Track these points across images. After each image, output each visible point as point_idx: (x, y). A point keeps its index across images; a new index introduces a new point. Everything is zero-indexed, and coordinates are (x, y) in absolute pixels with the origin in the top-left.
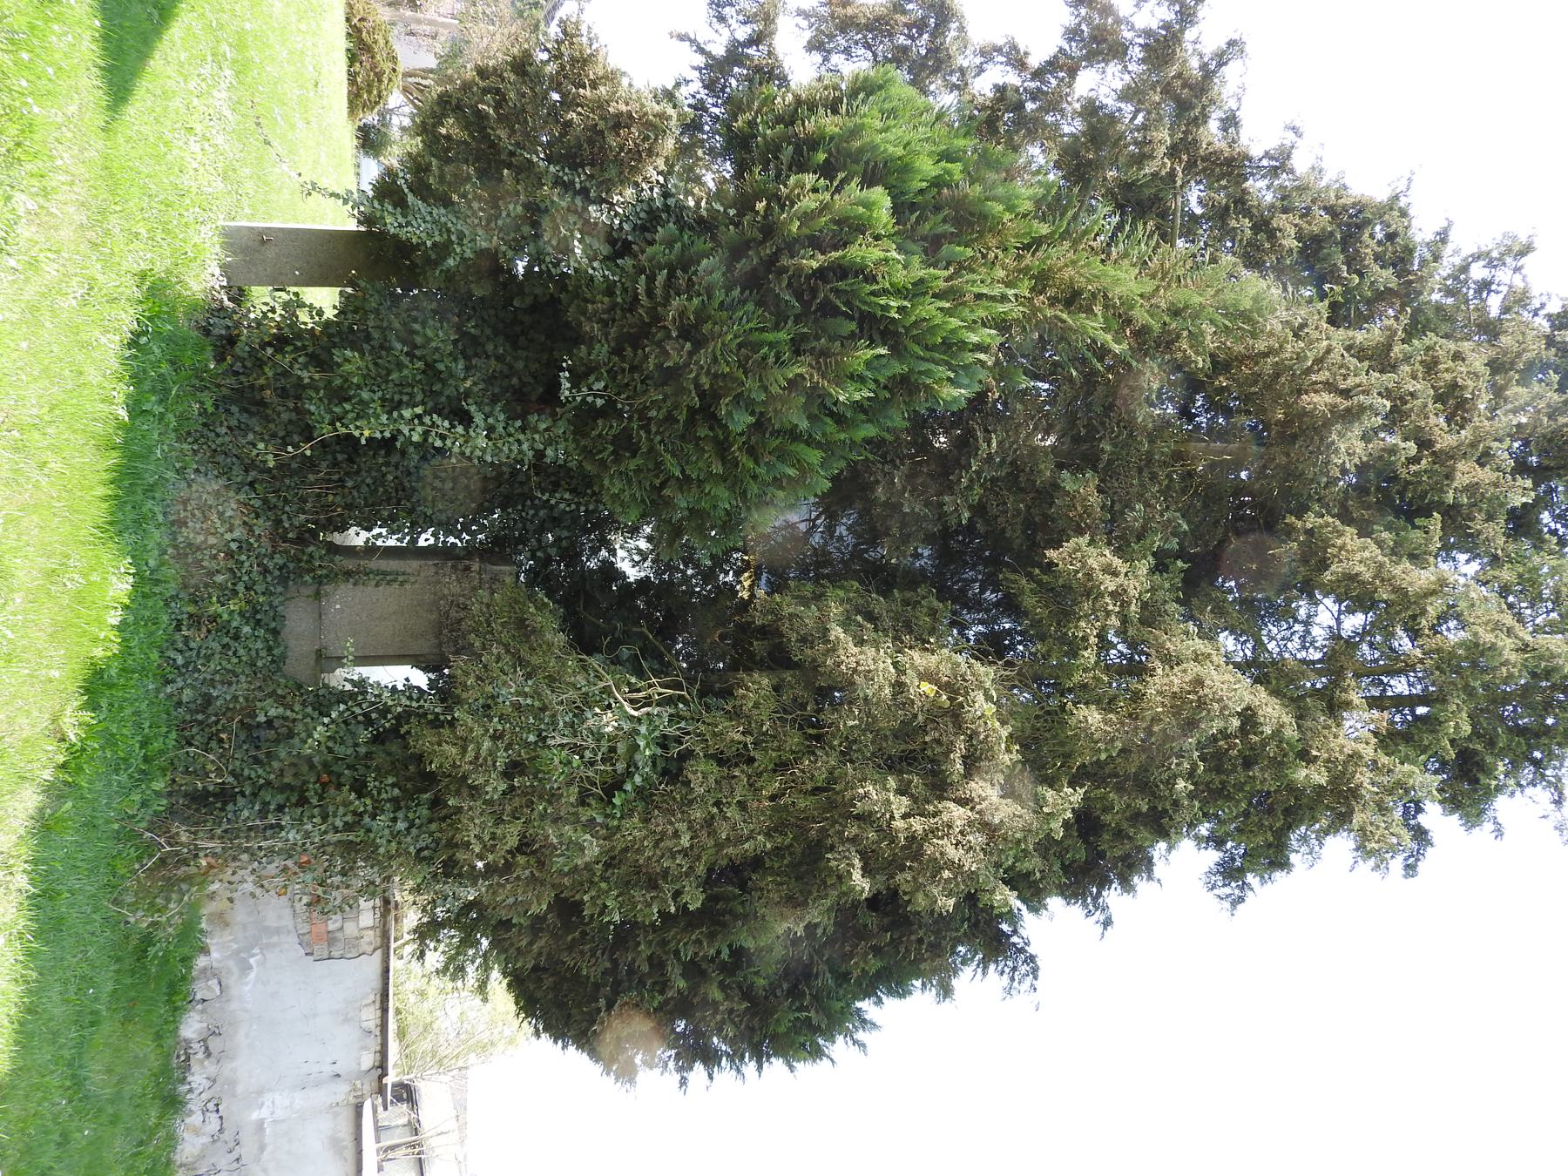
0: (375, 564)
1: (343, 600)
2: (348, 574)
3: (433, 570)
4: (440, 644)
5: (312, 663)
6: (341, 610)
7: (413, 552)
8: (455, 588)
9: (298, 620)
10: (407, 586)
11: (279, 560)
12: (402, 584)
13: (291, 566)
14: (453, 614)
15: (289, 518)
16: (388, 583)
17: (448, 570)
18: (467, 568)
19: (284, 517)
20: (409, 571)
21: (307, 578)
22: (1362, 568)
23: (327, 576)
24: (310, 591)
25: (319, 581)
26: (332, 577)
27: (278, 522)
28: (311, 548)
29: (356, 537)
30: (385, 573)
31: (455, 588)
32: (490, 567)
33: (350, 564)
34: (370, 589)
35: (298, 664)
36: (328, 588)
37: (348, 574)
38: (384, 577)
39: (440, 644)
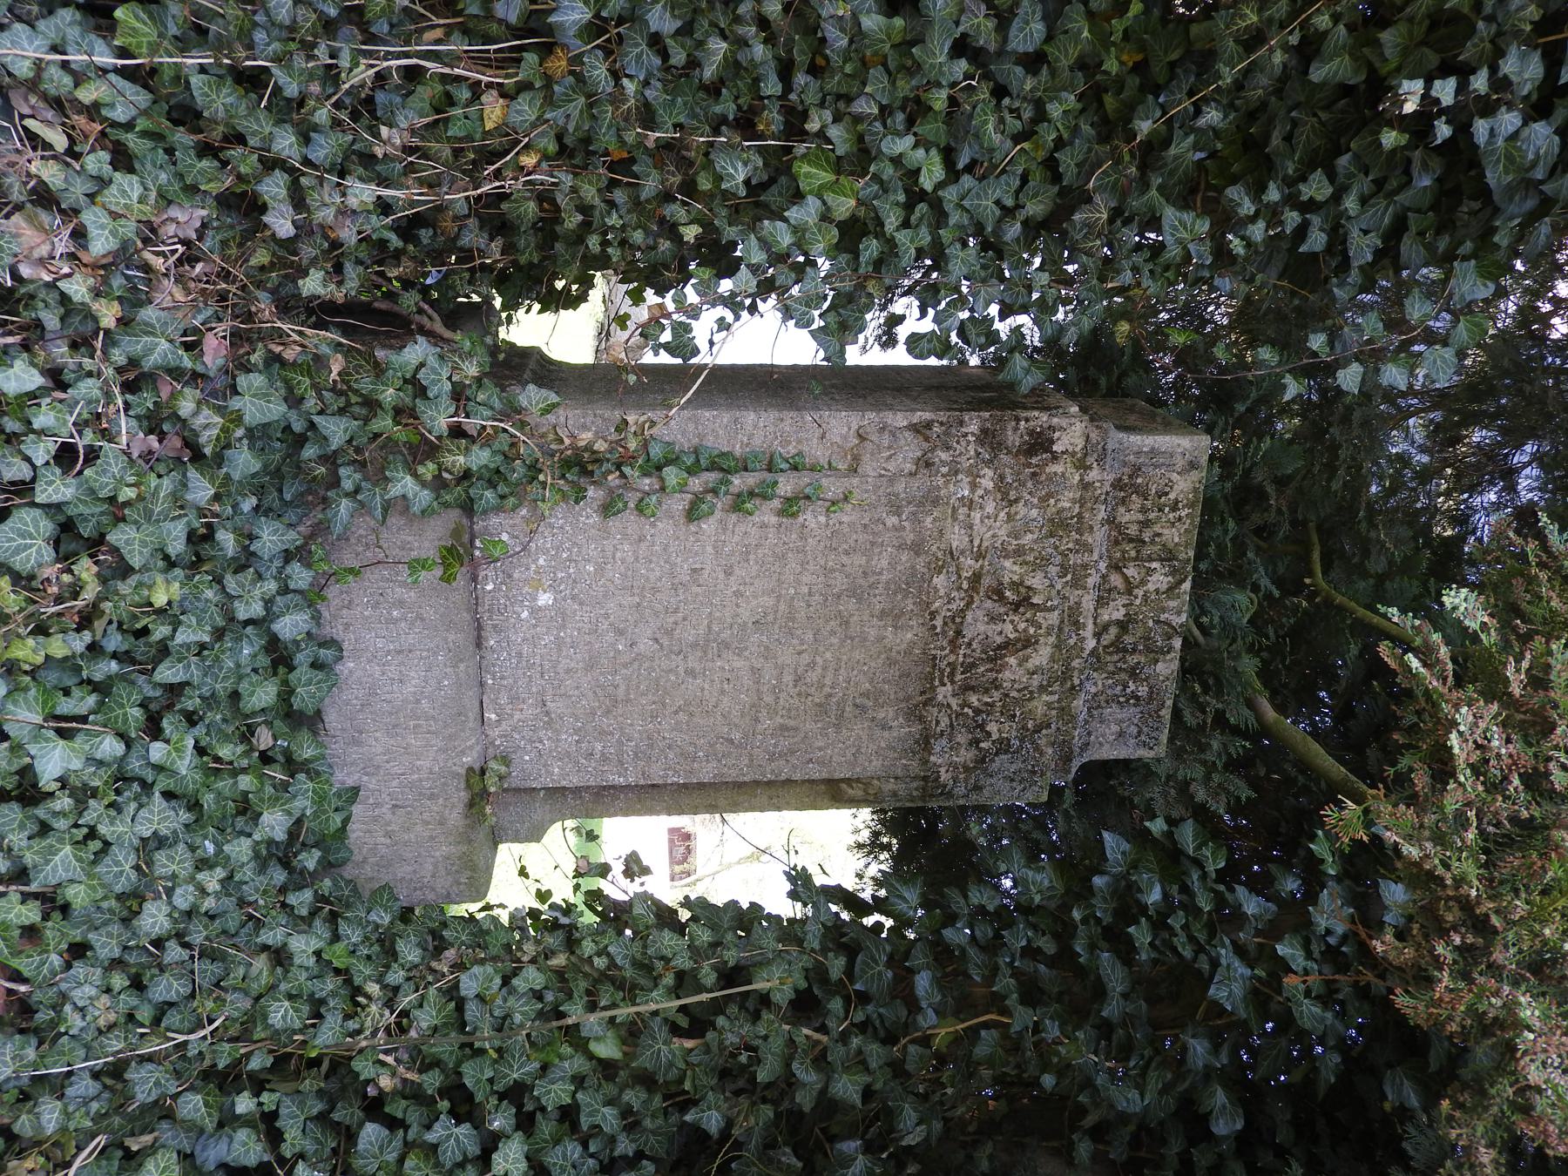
0: (680, 424)
1: (570, 578)
2: (580, 466)
3: (912, 447)
4: (925, 742)
5: (455, 817)
6: (560, 616)
7: (837, 384)
8: (990, 524)
9: (395, 679)
10: (812, 518)
11: (259, 402)
12: (791, 507)
13: (337, 430)
14: (977, 626)
15: (298, 199)
16: (738, 504)
17: (969, 450)
18: (1040, 443)
19: (274, 188)
20: (817, 452)
21: (404, 484)
22: (1530, 495)
23: (494, 477)
24: (428, 540)
25: (462, 495)
26: (512, 480)
27: (244, 206)
28: (417, 352)
29: (564, 334)
30: (724, 465)
31: (990, 524)
32: (1116, 438)
33: (584, 426)
34: (666, 528)
35: (395, 835)
36: (503, 528)
37: (580, 466)
38: (723, 479)
39: (925, 742)
